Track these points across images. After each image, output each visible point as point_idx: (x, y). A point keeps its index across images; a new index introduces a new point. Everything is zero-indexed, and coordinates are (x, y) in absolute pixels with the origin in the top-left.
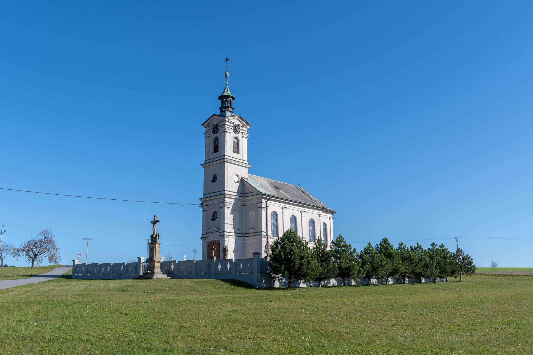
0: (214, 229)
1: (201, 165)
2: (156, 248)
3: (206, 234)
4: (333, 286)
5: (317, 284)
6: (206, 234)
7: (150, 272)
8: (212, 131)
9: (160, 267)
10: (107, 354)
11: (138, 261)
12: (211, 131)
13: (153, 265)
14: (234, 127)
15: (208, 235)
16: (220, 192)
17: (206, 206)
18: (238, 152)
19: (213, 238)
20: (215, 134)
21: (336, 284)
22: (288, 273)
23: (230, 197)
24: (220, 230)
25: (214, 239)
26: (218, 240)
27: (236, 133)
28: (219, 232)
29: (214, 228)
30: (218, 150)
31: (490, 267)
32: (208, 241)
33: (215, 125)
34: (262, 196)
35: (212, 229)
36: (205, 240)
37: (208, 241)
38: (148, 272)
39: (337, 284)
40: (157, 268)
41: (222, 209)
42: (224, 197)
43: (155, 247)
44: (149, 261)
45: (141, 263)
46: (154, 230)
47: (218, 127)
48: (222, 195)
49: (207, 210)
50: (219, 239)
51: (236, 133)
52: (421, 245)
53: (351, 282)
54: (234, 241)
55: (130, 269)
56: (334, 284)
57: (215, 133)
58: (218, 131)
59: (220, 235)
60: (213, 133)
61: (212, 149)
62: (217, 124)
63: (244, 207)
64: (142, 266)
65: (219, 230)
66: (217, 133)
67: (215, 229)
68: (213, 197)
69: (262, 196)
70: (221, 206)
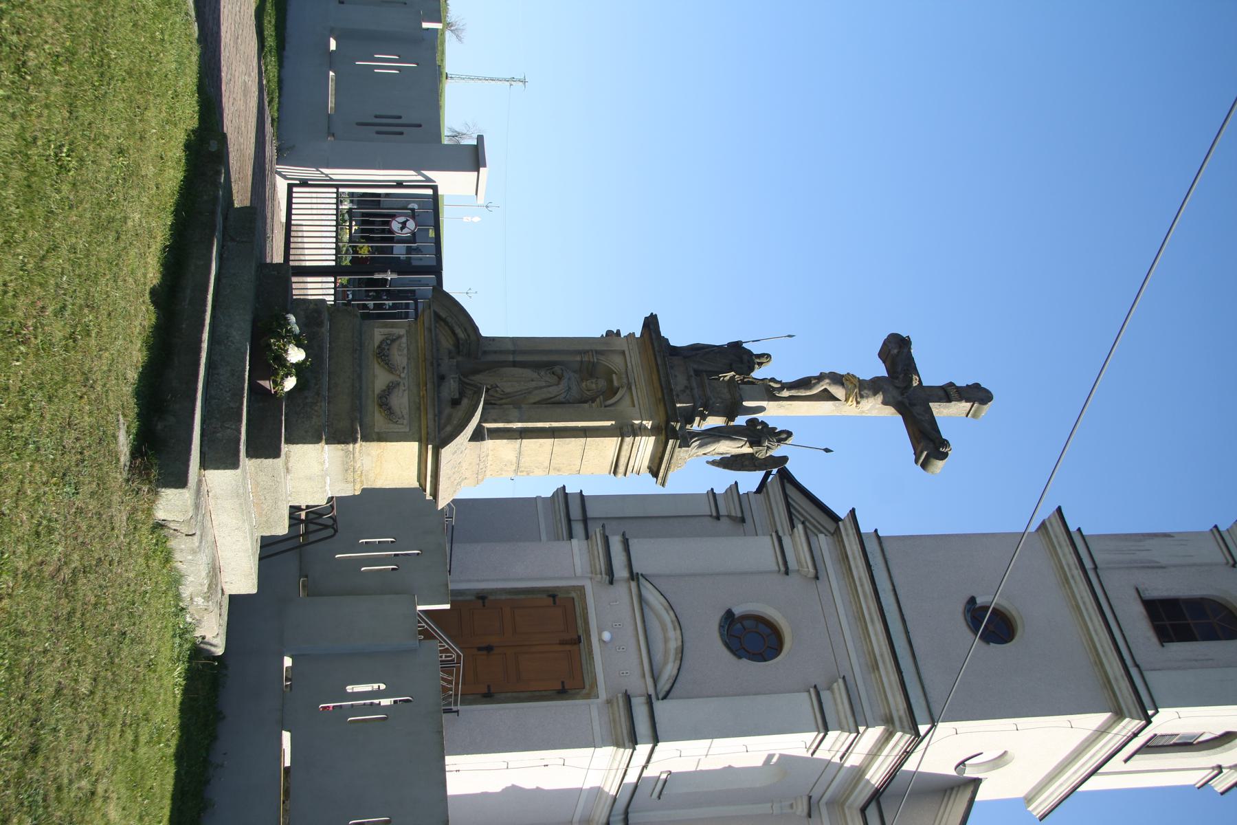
0: (666, 640)
1: (1059, 510)
2: (611, 443)
3: (633, 576)
6: (633, 576)
7: (290, 383)
9: (365, 491)
11: (435, 264)
13: (384, 402)
15: (622, 592)
16: (916, 678)
17: (811, 569)
19: (606, 636)
24: (665, 698)
25: (601, 640)
26: (594, 684)
28: (651, 691)
29: (673, 645)
31: (446, 132)
32: (581, 589)
35: (668, 618)
36: (593, 572)
37: (581, 589)
38: (281, 360)
40: (348, 468)
41: (803, 703)
42: (889, 722)
43: (625, 430)
44: (447, 343)
45: (430, 174)
46: (827, 396)
48: (902, 705)
49: (787, 573)
50: (603, 695)
54: (587, 786)
55: (386, 64)
59: (628, 698)
61: (1163, 587)
63: (802, 808)
64: (400, 184)
65: (664, 685)
67: (666, 652)
68: (879, 626)
70: (825, 695)
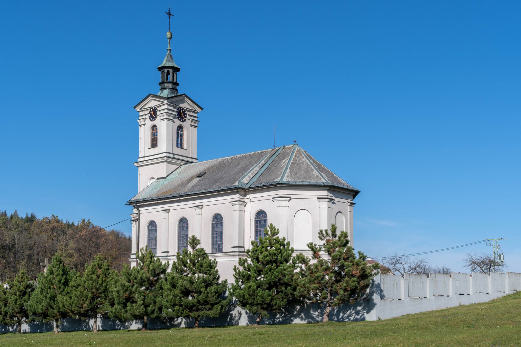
4: (25, 333)
5: (4, 330)
8: (148, 117)
10: (520, 332)
12: (147, 116)
14: (178, 112)
18: (181, 147)
20: (152, 121)
21: (29, 330)
22: (267, 286)
23: (278, 198)
27: (181, 120)
30: (157, 143)
33: (152, 108)
34: (138, 204)
39: (31, 330)
47: (156, 112)
51: (181, 120)
52: (362, 252)
53: (9, 330)
56: (25, 330)
57: (152, 119)
58: (156, 117)
60: (150, 119)
62: (155, 107)
66: (155, 120)
69: (138, 204)
